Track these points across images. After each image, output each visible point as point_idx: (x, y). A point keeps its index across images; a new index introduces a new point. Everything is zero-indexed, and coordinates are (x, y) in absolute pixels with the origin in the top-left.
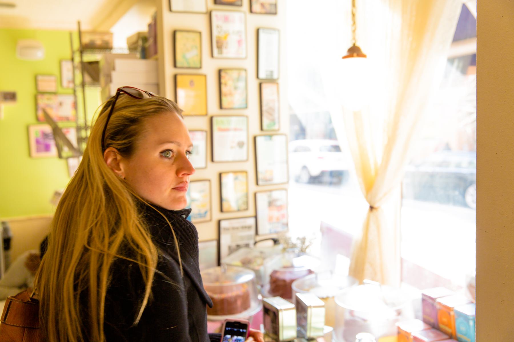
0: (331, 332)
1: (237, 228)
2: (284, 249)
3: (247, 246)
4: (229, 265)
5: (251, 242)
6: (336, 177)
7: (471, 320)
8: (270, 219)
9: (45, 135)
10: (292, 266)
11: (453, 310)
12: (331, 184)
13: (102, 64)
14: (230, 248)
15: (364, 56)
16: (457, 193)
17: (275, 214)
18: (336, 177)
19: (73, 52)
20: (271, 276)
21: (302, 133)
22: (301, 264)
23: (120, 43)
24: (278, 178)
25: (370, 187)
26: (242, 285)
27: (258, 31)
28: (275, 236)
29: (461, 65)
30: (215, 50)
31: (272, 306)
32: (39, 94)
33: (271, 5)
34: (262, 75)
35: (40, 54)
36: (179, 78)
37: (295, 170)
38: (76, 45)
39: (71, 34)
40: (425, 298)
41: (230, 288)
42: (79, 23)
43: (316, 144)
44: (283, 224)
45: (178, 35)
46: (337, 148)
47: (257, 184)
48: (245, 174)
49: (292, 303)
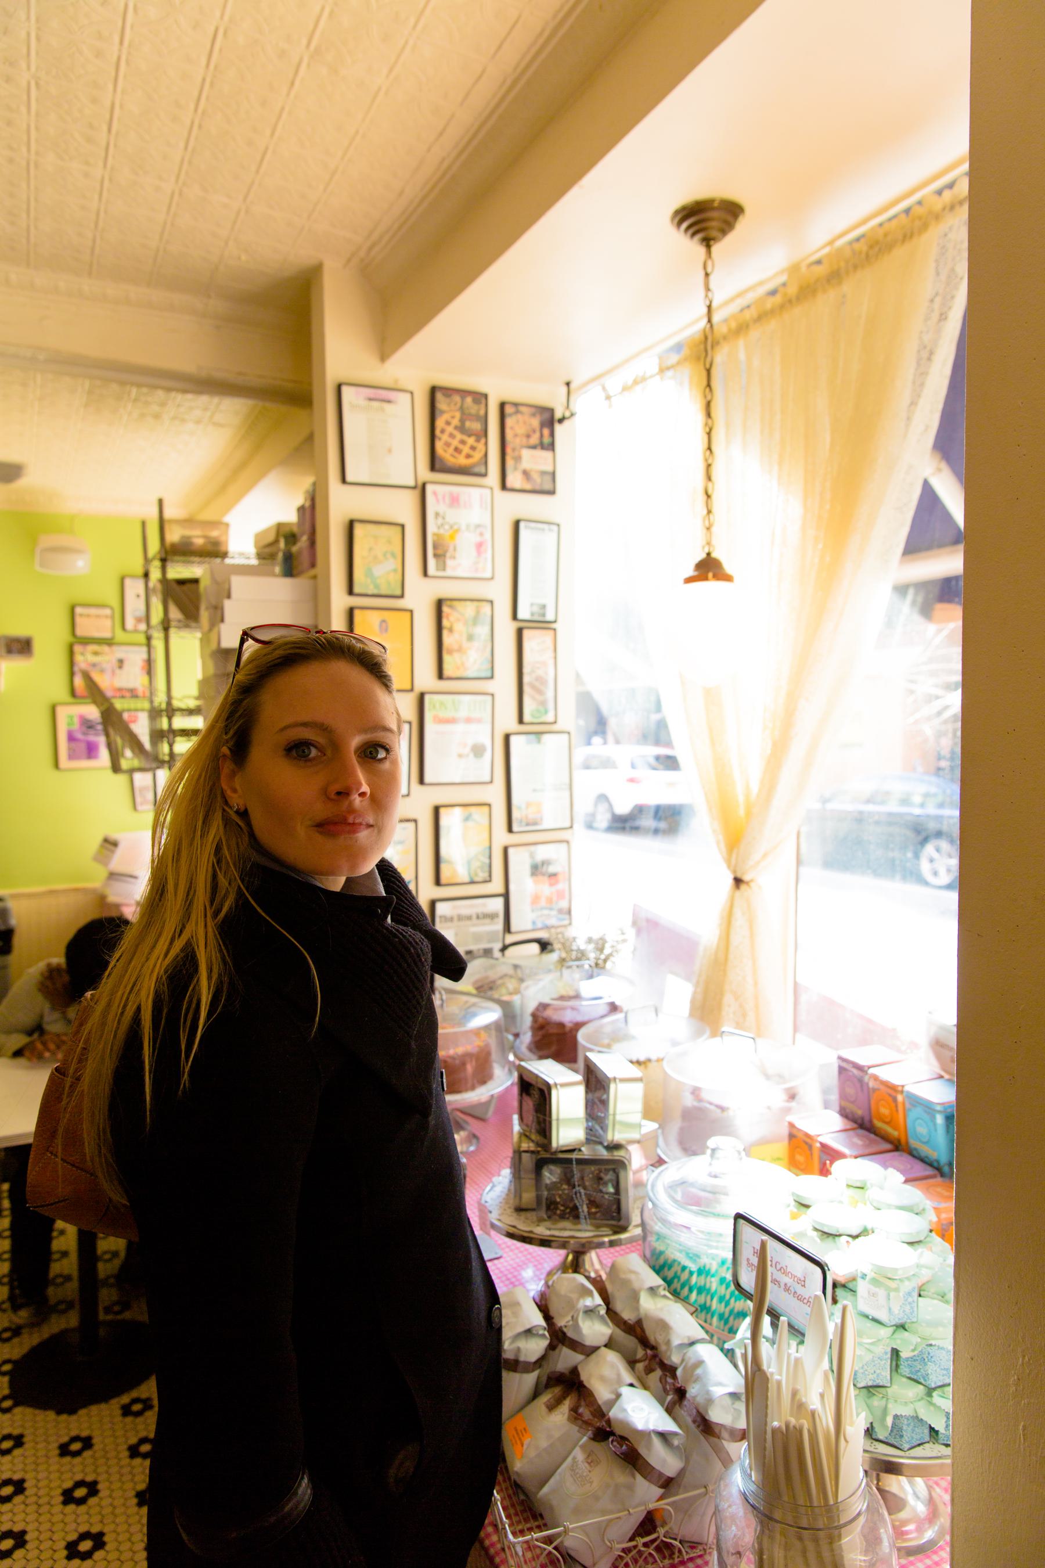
1: (469, 918)
2: (562, 961)
3: (488, 953)
5: (498, 946)
6: (668, 819)
7: (939, 1112)
9: (87, 724)
10: (577, 997)
11: (902, 1092)
15: (728, 578)
17: (546, 889)
18: (668, 819)
19: (147, 560)
20: (534, 1015)
22: (595, 991)
23: (242, 543)
24: (552, 816)
25: (735, 841)
26: (477, 1032)
27: (517, 525)
28: (543, 935)
29: (920, 599)
31: (537, 1076)
32: (76, 642)
33: (543, 473)
35: (80, 563)
38: (154, 547)
39: (144, 524)
40: (844, 1065)
42: (161, 502)
44: (560, 911)
45: (359, 530)
47: (510, 830)
48: (486, 809)
49: (576, 1071)
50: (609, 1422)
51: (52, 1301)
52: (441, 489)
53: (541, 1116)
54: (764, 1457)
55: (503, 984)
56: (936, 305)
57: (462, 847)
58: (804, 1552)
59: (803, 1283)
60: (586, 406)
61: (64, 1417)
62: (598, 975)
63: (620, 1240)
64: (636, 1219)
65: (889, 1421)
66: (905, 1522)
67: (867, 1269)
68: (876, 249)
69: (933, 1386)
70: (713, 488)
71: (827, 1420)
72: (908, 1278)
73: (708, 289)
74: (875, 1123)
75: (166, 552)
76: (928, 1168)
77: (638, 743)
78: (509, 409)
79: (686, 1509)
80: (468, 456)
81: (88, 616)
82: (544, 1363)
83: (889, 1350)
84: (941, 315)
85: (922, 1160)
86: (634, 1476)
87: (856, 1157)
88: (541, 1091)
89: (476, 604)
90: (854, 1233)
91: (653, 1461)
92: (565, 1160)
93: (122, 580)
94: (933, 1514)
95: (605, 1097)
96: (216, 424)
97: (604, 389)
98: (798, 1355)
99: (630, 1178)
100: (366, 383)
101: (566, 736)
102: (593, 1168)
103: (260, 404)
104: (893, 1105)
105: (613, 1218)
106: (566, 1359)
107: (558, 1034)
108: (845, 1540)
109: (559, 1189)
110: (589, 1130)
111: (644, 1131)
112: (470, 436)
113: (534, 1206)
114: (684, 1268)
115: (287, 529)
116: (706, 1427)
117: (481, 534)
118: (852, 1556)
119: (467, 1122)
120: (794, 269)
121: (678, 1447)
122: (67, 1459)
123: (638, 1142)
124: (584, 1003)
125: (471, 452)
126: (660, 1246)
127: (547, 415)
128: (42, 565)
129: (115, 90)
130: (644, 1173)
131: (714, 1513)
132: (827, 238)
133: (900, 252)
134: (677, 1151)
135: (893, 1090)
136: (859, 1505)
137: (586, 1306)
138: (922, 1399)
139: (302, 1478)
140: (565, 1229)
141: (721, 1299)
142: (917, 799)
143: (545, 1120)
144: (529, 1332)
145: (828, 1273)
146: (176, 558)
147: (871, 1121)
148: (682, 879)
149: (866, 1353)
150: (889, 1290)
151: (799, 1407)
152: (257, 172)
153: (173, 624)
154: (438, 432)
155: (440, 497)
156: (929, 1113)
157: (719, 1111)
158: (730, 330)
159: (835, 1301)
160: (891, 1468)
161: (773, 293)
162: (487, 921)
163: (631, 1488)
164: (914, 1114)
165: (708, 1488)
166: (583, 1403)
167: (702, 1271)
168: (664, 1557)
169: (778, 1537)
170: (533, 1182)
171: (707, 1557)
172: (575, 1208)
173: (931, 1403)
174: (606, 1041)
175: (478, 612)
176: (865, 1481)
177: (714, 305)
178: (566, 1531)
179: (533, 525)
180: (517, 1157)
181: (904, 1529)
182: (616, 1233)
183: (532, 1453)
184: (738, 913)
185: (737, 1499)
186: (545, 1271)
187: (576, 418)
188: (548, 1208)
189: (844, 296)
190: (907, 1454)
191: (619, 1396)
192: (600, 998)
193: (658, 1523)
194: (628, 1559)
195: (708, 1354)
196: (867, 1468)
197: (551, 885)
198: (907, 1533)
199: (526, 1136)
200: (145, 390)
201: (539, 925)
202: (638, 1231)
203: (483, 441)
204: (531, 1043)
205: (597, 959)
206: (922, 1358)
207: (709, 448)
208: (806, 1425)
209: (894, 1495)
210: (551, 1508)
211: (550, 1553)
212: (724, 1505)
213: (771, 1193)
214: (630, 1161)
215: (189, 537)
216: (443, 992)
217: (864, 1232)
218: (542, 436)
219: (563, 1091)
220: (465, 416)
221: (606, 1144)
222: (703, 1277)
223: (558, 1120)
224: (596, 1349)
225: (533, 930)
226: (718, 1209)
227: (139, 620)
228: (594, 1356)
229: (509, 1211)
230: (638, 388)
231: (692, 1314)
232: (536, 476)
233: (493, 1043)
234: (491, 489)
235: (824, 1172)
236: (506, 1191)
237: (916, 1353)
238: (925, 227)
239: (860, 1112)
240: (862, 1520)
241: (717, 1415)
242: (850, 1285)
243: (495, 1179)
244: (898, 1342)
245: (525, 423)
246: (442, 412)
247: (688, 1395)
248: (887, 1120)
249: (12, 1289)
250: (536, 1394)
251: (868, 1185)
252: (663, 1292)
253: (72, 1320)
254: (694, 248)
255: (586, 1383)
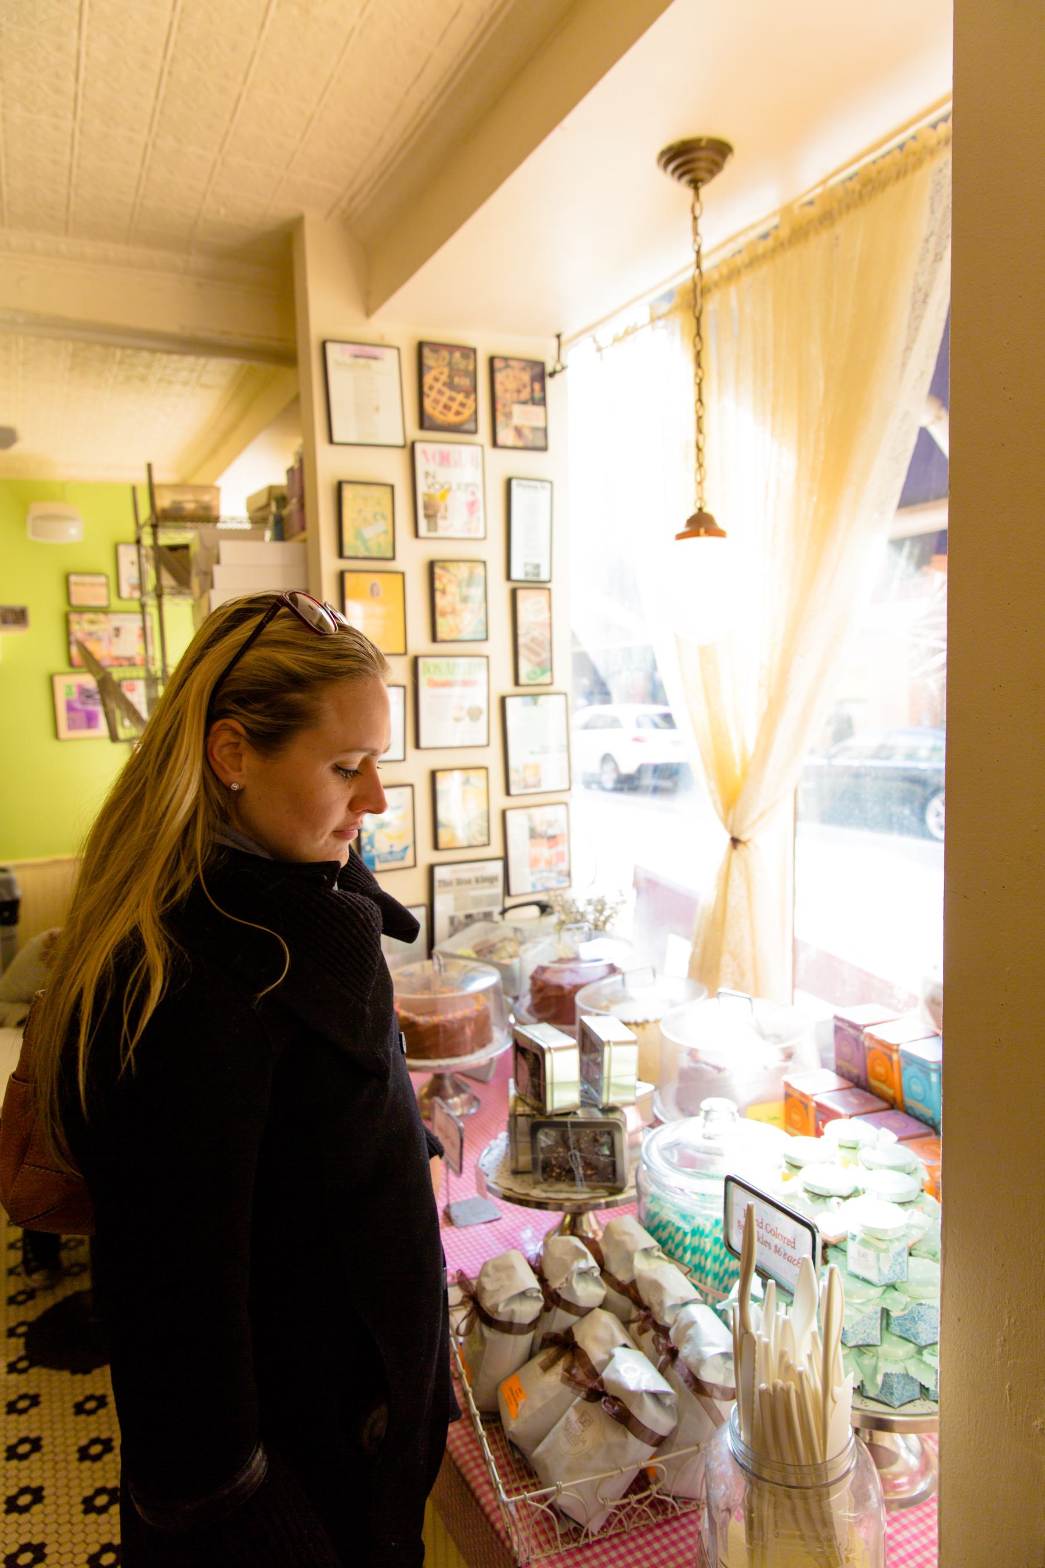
0: (652, 1092)
1: (469, 882)
2: (562, 923)
3: (487, 916)
4: (447, 955)
5: (498, 909)
6: (665, 778)
7: (934, 1070)
8: (534, 862)
9: (84, 693)
10: (576, 959)
11: (897, 1051)
12: (656, 790)
13: (195, 549)
14: (452, 920)
15: (721, 534)
16: (907, 812)
17: (544, 852)
18: (665, 778)
19: (139, 527)
20: (533, 978)
21: (600, 691)
22: (593, 953)
23: (234, 506)
24: (553, 779)
25: (732, 801)
26: (475, 996)
27: (509, 483)
28: (542, 897)
29: (916, 551)
30: (423, 523)
31: (531, 1041)
32: (72, 611)
33: (535, 429)
34: (517, 573)
35: (74, 531)
36: (349, 579)
37: (586, 762)
38: (145, 513)
39: (134, 489)
40: (840, 1024)
41: (453, 1003)
42: (149, 467)
43: (628, 711)
44: (560, 873)
45: (348, 492)
46: (668, 718)
47: (508, 793)
48: (483, 772)
49: (571, 1034)
50: (601, 1383)
51: (66, 1264)
52: (430, 448)
53: (536, 1080)
54: (753, 1418)
55: (503, 948)
56: (931, 245)
57: (462, 809)
58: (793, 1511)
59: (792, 1244)
60: (577, 359)
61: (79, 1377)
62: (596, 938)
63: (616, 1201)
64: (631, 1181)
65: (879, 1379)
66: (897, 1476)
67: (857, 1230)
68: (869, 188)
69: (923, 1344)
70: (704, 439)
71: (815, 1381)
72: (897, 1239)
73: (696, 233)
74: (871, 1083)
75: (157, 518)
76: (924, 1126)
77: (643, 702)
78: (498, 364)
79: (678, 1466)
80: (458, 413)
81: (83, 584)
82: (539, 1324)
83: (879, 1309)
84: (936, 255)
85: (918, 1118)
86: (626, 1437)
87: (851, 1117)
88: (536, 1056)
89: (468, 565)
90: (845, 1194)
91: (645, 1421)
92: (560, 1123)
93: (116, 547)
94: (925, 1468)
95: (599, 1060)
96: (204, 386)
97: (595, 341)
98: (787, 1317)
99: (625, 1140)
100: (357, 340)
101: (563, 697)
102: (588, 1131)
103: (247, 364)
104: (888, 1064)
105: (609, 1180)
106: (561, 1320)
107: (557, 997)
108: (834, 1498)
109: (554, 1152)
110: (584, 1093)
111: (639, 1093)
112: (458, 392)
113: (530, 1168)
114: (678, 1229)
115: (278, 493)
116: (698, 1386)
117: (473, 493)
118: (840, 1512)
119: (467, 1085)
120: (786, 211)
121: (670, 1406)
122: (83, 1417)
123: (633, 1104)
124: (583, 965)
125: (461, 409)
126: (654, 1208)
127: (537, 370)
128: (35, 533)
129: (80, 38)
130: (641, 1134)
131: (705, 1475)
132: (819, 177)
133: (893, 190)
134: (675, 1112)
135: (889, 1049)
136: (848, 1463)
137: (580, 1268)
138: (913, 1356)
139: (257, 1451)
140: (561, 1191)
141: (716, 1259)
142: (923, 753)
143: (539, 1084)
144: (523, 1295)
145: (817, 1235)
146: (169, 524)
147: (867, 1080)
148: (681, 842)
149: (854, 1312)
150: (878, 1251)
151: (787, 1368)
152: (232, 120)
153: (166, 591)
154: (426, 389)
155: (430, 456)
156: (923, 1072)
157: (715, 1071)
158: (721, 276)
159: (825, 1261)
160: (882, 1425)
161: (765, 236)
162: (487, 884)
163: (623, 1447)
164: (910, 1071)
165: (700, 1446)
166: (577, 1364)
167: (696, 1232)
168: (658, 1513)
169: (767, 1495)
170: (529, 1145)
171: (700, 1512)
172: (570, 1171)
173: (921, 1361)
174: (604, 1003)
175: (471, 574)
176: (853, 1439)
177: (704, 251)
178: (559, 1491)
179: (525, 482)
180: (513, 1122)
181: (896, 1482)
182: (611, 1194)
183: (526, 1413)
184: (735, 873)
185: (727, 1459)
186: (543, 1232)
187: (568, 372)
188: (544, 1171)
189: (837, 238)
190: (898, 1411)
191: (612, 1356)
192: (600, 960)
193: (652, 1479)
194: (621, 1515)
195: (701, 1315)
196: (857, 1425)
197: (550, 847)
198: (899, 1485)
199: (522, 1100)
200: (129, 352)
201: (539, 887)
202: (633, 1192)
203: (472, 397)
204: (530, 1006)
205: (596, 920)
206: (912, 1317)
207: (700, 400)
208: (793, 1386)
209: (887, 1449)
210: (545, 1468)
211: (543, 1511)
212: (714, 1464)
213: (761, 1153)
214: (625, 1124)
215: (180, 502)
216: (441, 957)
217: (855, 1193)
218: (533, 390)
219: (556, 1055)
220: (453, 372)
221: (601, 1107)
222: (697, 1237)
223: (552, 1084)
224: (590, 1310)
225: (533, 893)
226: (712, 1170)
227: (133, 588)
228: (588, 1317)
229: (506, 1174)
230: (629, 339)
231: (686, 1275)
232: (527, 432)
233: (491, 1005)
234: (482, 446)
235: (819, 1133)
236: (503, 1154)
237: (906, 1312)
238: (919, 162)
239: (855, 1071)
240: (851, 1477)
241: (709, 1375)
242: (841, 1246)
243: (493, 1143)
244: (889, 1301)
245: (515, 377)
246: (430, 368)
247: (680, 1356)
248: (883, 1078)
249: (25, 1254)
250: (531, 1355)
251: (860, 1145)
252: (657, 1253)
253: (84, 1283)
254: (682, 190)
255: (580, 1344)
